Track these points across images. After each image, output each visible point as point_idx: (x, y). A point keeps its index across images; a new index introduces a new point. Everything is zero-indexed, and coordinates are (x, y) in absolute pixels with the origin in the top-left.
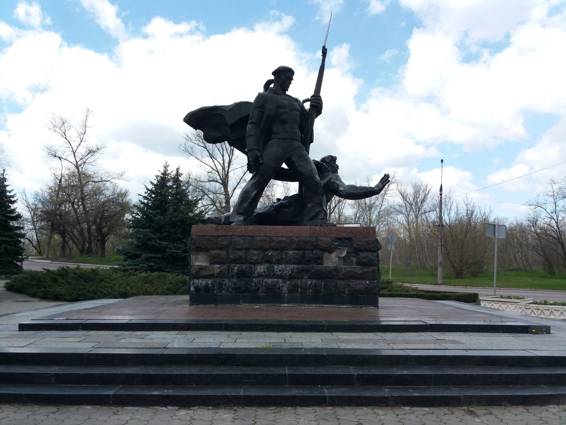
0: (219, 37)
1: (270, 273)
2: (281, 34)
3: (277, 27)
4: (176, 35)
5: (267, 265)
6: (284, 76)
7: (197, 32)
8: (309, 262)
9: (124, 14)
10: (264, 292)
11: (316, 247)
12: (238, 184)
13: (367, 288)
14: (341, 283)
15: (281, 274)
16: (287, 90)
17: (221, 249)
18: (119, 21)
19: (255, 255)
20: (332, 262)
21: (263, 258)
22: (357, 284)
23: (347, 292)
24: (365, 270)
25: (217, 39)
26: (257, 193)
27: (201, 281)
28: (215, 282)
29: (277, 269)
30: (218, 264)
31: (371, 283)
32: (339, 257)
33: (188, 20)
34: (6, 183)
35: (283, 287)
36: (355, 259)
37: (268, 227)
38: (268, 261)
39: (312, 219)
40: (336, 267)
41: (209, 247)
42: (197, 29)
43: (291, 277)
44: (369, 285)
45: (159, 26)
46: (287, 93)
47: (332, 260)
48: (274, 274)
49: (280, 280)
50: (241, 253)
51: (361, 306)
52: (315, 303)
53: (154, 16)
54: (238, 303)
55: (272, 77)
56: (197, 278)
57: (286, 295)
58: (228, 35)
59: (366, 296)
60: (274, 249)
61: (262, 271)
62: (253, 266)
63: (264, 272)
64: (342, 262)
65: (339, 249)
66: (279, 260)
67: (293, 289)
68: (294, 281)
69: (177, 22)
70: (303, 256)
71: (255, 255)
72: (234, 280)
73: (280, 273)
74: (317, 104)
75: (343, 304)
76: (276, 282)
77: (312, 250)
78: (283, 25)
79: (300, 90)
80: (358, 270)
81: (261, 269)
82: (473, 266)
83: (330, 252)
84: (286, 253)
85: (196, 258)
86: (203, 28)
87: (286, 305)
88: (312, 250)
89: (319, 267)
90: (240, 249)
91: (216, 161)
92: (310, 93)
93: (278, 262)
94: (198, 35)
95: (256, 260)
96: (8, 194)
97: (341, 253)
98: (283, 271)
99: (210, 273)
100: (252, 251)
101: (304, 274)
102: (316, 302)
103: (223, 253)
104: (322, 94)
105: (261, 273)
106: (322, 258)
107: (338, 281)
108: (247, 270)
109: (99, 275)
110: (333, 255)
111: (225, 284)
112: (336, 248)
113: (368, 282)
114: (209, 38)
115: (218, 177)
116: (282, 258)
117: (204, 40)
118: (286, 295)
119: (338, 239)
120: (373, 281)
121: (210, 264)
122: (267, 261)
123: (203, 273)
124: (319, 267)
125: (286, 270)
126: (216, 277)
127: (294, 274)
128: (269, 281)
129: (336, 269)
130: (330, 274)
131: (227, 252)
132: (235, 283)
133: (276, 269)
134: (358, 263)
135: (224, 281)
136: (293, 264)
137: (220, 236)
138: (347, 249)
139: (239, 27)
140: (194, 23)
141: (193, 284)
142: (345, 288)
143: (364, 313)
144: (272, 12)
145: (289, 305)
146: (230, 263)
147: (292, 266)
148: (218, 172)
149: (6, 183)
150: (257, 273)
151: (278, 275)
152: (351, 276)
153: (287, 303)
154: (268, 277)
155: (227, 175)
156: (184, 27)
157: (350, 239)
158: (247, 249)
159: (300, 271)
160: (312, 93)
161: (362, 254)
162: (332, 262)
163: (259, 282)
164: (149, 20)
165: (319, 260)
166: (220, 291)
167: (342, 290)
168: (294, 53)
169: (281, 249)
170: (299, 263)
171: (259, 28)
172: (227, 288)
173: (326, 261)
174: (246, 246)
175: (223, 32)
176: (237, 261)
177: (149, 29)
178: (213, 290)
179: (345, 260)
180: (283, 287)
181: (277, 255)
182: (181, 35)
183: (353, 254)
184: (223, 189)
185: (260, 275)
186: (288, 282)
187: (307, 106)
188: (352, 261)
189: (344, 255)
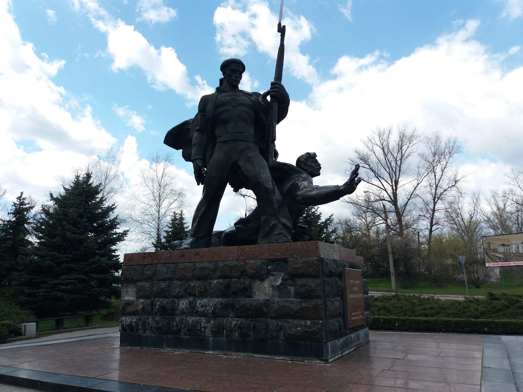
0: (404, 61)
1: (192, 310)
2: (467, 40)
3: (462, 34)
4: (361, 68)
5: (191, 299)
7: (381, 60)
8: (235, 294)
9: (315, 62)
10: (186, 335)
11: (243, 273)
12: (409, 199)
13: (306, 332)
14: (273, 323)
15: (203, 311)
17: (146, 280)
18: (311, 67)
19: (177, 286)
20: (265, 294)
21: (186, 290)
22: (293, 326)
23: (282, 337)
24: (304, 305)
25: (403, 63)
26: (205, 209)
27: (127, 318)
28: (140, 320)
29: (200, 304)
30: (144, 298)
31: (313, 323)
32: (273, 287)
33: (371, 51)
34: (184, 221)
35: (205, 328)
36: (293, 288)
38: (189, 293)
39: (267, 235)
40: (268, 300)
41: (135, 278)
42: (381, 57)
43: (215, 315)
44: (310, 328)
45: (345, 64)
47: (264, 291)
48: (197, 312)
49: (203, 318)
50: (163, 285)
51: (302, 358)
52: (244, 352)
53: (340, 57)
54: (161, 347)
56: (125, 315)
57: (211, 339)
58: (413, 56)
59: (308, 343)
60: (198, 279)
62: (176, 300)
63: (186, 308)
64: (277, 293)
65: (273, 275)
66: (202, 292)
67: (218, 331)
68: (219, 319)
69: (361, 56)
70: (228, 286)
71: (177, 286)
72: (158, 318)
73: (202, 310)
75: (279, 354)
76: (197, 322)
77: (239, 278)
78: (467, 30)
80: (293, 303)
81: (183, 304)
83: (262, 280)
84: (210, 283)
85: (127, 291)
86: (386, 54)
87: (211, 352)
88: (239, 278)
89: (244, 301)
90: (163, 280)
91: (383, 181)
93: (202, 295)
94: (382, 64)
95: (179, 292)
96: (186, 230)
97: (276, 280)
98: (206, 306)
99: (135, 309)
100: (175, 282)
101: (230, 311)
102: (244, 350)
103: (147, 284)
105: (183, 309)
106: (251, 289)
107: (270, 321)
108: (167, 306)
110: (266, 284)
111: (149, 323)
112: (268, 273)
113: (309, 323)
114: (394, 63)
115: (386, 195)
116: (206, 290)
117: (389, 66)
118: (211, 339)
119: (272, 261)
120: (316, 321)
121: (137, 298)
122: (190, 295)
123: (130, 309)
124: (244, 301)
125: (209, 306)
126: (141, 314)
127: (217, 311)
128: (191, 320)
129: (267, 304)
130: (260, 312)
131: (152, 284)
132: (157, 322)
133: (198, 304)
134: (298, 295)
135: (148, 319)
136: (217, 297)
137: (146, 265)
138: (282, 274)
139: (421, 45)
140: (377, 53)
142: (279, 331)
144: (455, 22)
145: (214, 353)
146: (155, 297)
147: (216, 300)
148: (385, 190)
149: (184, 221)
151: (200, 312)
152: (285, 314)
153: (213, 350)
154: (191, 314)
155: (395, 194)
156: (368, 59)
157: (285, 261)
158: (170, 279)
159: (225, 307)
161: (299, 282)
162: (265, 294)
163: (181, 322)
164: (336, 61)
165: (247, 291)
166: (145, 332)
167: (274, 334)
168: (486, 56)
169: (205, 277)
170: (224, 295)
171: (441, 40)
172: (151, 327)
173: (257, 293)
174: (169, 275)
175: (408, 55)
176: (161, 294)
177: (336, 70)
178: (138, 330)
179: (280, 289)
180: (205, 328)
181: (200, 286)
182: (366, 67)
183: (290, 282)
184: (393, 207)
186: (212, 322)
188: (289, 292)
189: (278, 284)
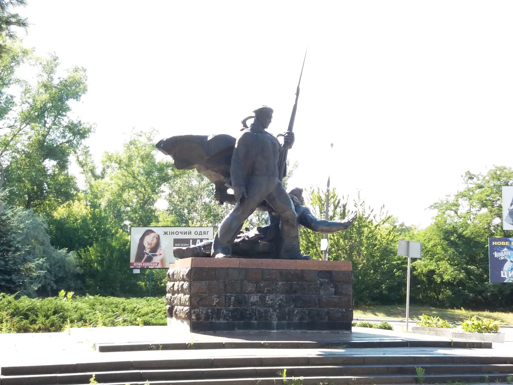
5: (259, 294)
6: (263, 116)
16: (267, 128)
35: (273, 315)
37: (259, 259)
46: (266, 130)
55: (254, 115)
61: (254, 301)
74: (290, 139)
79: (276, 129)
82: (392, 233)
87: (275, 331)
92: (285, 130)
93: (270, 292)
102: (300, 329)
104: (294, 131)
109: (87, 216)
111: (223, 313)
122: (259, 292)
141: (194, 313)
143: (341, 335)
150: (251, 303)
160: (286, 131)
172: (225, 316)
185: (253, 304)
187: (281, 141)
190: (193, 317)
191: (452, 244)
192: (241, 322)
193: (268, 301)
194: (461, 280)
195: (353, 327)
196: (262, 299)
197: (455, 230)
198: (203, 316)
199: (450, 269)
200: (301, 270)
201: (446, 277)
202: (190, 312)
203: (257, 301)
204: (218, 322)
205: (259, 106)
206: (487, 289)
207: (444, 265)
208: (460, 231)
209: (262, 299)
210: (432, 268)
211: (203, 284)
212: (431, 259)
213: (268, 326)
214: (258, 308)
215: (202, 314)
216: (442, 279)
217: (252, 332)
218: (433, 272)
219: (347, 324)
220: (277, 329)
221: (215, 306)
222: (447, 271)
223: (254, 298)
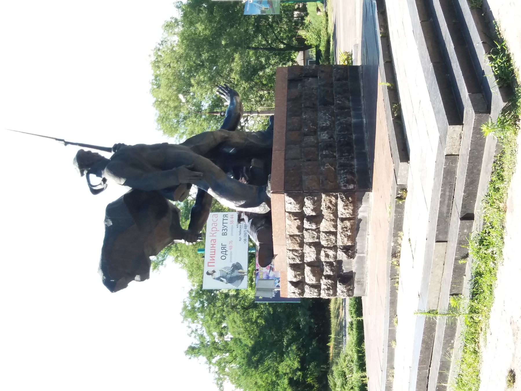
87: (364, 120)
102: (360, 101)
141: (345, 186)
190: (351, 187)
191: (260, 361)
192: (355, 146)
193: (327, 124)
194: (298, 349)
195: (354, 64)
196: (323, 129)
197: (249, 358)
198: (349, 177)
199: (288, 361)
200: (287, 101)
201: (296, 365)
202: (344, 192)
203: (327, 133)
204: (356, 167)
205: (75, 169)
206: (307, 323)
207: (283, 368)
208: (247, 351)
209: (323, 129)
210: (286, 381)
211: (308, 181)
212: (278, 385)
213: (359, 126)
214: (336, 132)
215: (346, 177)
216: (298, 369)
217: (366, 136)
218: (291, 381)
219: (350, 70)
220: (362, 118)
221: (335, 168)
222: (290, 364)
223: (324, 136)
